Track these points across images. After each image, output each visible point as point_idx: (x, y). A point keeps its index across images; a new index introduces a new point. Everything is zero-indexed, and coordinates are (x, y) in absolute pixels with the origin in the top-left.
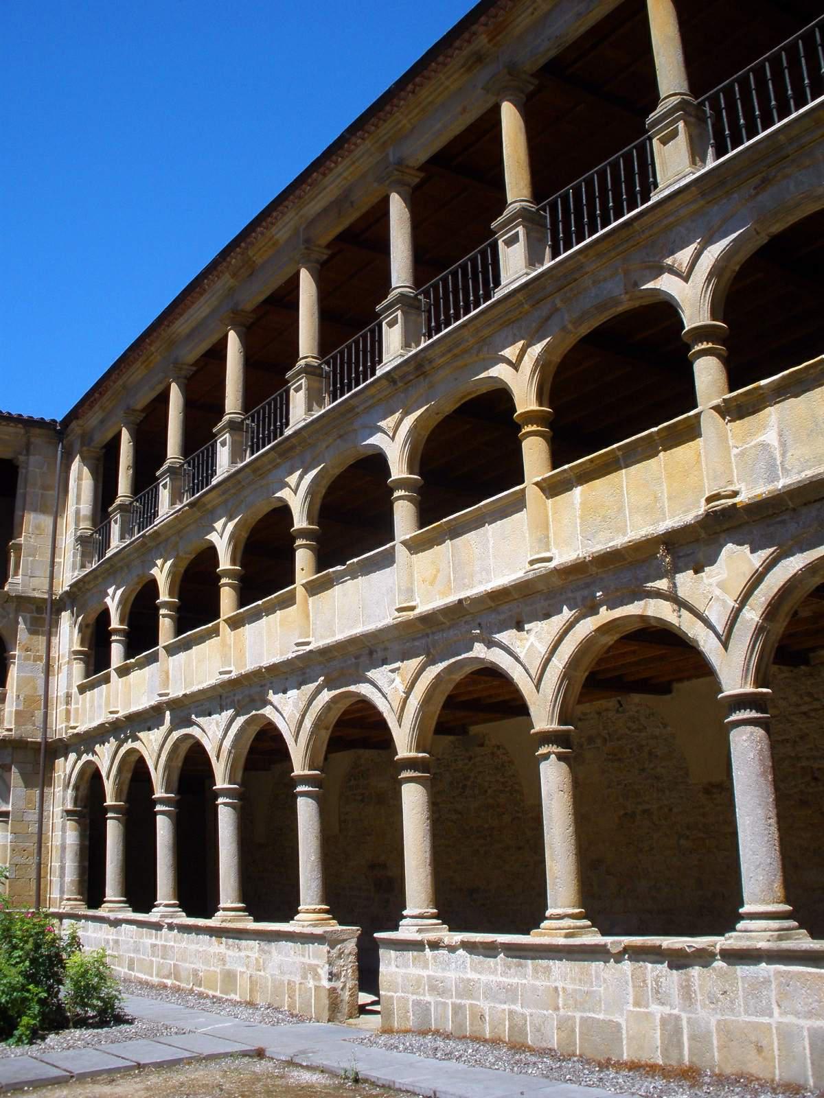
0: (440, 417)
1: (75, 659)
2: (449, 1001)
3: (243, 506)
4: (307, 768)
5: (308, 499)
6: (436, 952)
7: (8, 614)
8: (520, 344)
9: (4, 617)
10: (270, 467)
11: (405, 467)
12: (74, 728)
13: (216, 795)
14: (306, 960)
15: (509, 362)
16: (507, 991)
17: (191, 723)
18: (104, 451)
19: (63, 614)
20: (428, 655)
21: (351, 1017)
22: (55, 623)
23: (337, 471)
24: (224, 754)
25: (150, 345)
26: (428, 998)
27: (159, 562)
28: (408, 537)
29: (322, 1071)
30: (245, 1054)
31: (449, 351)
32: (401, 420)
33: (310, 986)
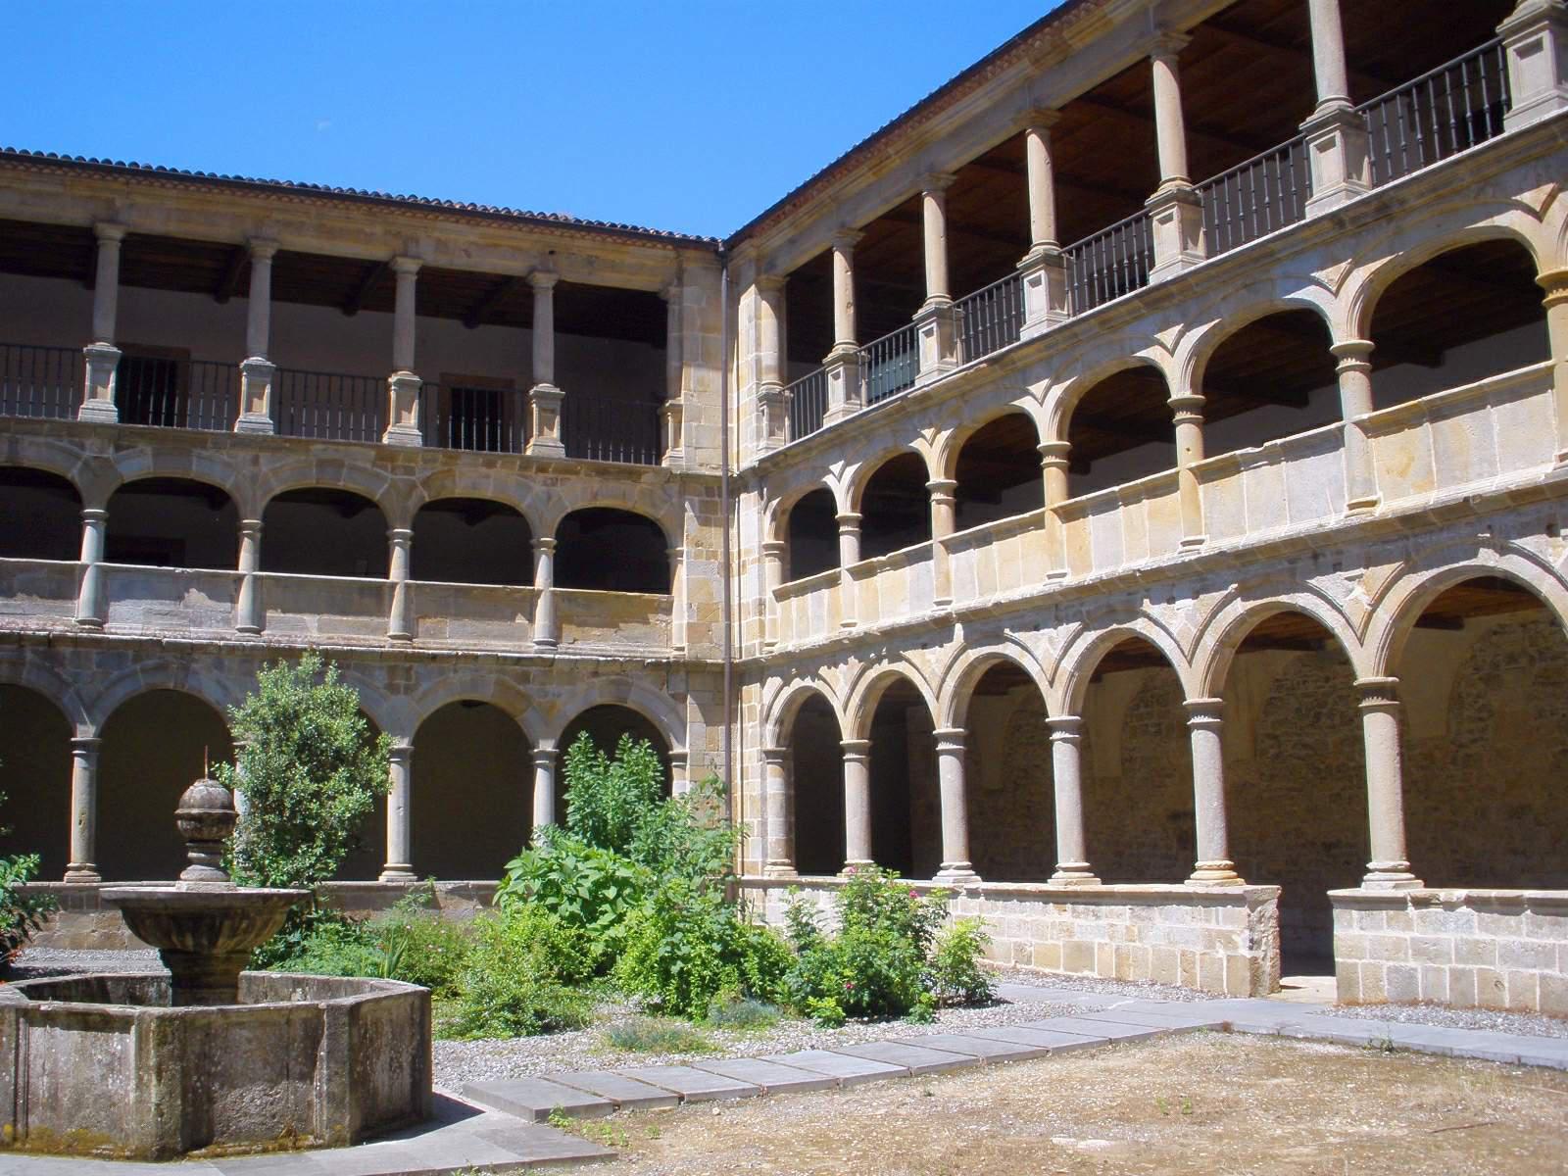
0: (1403, 271)
1: (767, 555)
2: (1446, 967)
3: (1079, 366)
4: (1206, 694)
5: (1192, 362)
6: (1424, 910)
7: (670, 497)
8: (1548, 188)
9: (666, 502)
10: (1128, 318)
11: (1355, 331)
12: (772, 645)
13: (1051, 728)
14: (1213, 926)
15: (1528, 210)
16: (1537, 953)
17: (1001, 639)
18: (788, 279)
19: (743, 496)
20: (1407, 562)
21: (1272, 992)
22: (731, 509)
23: (1233, 329)
24: (1062, 678)
25: (887, 145)
26: (1412, 964)
27: (928, 433)
28: (1365, 416)
29: (1331, 1043)
30: (1212, 1028)
31: (1434, 190)
32: (1349, 273)
33: (1220, 956)
